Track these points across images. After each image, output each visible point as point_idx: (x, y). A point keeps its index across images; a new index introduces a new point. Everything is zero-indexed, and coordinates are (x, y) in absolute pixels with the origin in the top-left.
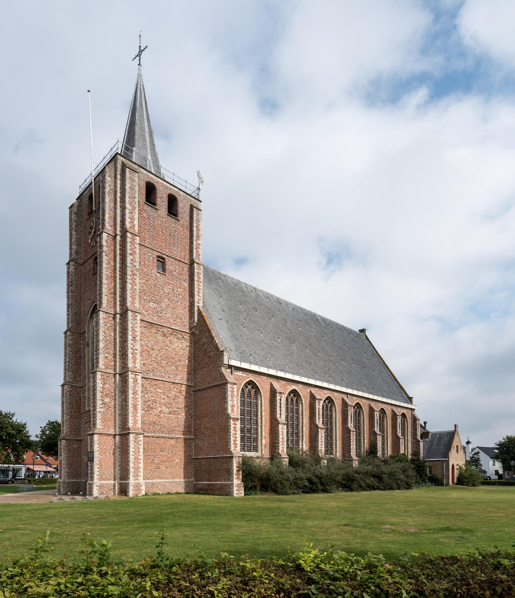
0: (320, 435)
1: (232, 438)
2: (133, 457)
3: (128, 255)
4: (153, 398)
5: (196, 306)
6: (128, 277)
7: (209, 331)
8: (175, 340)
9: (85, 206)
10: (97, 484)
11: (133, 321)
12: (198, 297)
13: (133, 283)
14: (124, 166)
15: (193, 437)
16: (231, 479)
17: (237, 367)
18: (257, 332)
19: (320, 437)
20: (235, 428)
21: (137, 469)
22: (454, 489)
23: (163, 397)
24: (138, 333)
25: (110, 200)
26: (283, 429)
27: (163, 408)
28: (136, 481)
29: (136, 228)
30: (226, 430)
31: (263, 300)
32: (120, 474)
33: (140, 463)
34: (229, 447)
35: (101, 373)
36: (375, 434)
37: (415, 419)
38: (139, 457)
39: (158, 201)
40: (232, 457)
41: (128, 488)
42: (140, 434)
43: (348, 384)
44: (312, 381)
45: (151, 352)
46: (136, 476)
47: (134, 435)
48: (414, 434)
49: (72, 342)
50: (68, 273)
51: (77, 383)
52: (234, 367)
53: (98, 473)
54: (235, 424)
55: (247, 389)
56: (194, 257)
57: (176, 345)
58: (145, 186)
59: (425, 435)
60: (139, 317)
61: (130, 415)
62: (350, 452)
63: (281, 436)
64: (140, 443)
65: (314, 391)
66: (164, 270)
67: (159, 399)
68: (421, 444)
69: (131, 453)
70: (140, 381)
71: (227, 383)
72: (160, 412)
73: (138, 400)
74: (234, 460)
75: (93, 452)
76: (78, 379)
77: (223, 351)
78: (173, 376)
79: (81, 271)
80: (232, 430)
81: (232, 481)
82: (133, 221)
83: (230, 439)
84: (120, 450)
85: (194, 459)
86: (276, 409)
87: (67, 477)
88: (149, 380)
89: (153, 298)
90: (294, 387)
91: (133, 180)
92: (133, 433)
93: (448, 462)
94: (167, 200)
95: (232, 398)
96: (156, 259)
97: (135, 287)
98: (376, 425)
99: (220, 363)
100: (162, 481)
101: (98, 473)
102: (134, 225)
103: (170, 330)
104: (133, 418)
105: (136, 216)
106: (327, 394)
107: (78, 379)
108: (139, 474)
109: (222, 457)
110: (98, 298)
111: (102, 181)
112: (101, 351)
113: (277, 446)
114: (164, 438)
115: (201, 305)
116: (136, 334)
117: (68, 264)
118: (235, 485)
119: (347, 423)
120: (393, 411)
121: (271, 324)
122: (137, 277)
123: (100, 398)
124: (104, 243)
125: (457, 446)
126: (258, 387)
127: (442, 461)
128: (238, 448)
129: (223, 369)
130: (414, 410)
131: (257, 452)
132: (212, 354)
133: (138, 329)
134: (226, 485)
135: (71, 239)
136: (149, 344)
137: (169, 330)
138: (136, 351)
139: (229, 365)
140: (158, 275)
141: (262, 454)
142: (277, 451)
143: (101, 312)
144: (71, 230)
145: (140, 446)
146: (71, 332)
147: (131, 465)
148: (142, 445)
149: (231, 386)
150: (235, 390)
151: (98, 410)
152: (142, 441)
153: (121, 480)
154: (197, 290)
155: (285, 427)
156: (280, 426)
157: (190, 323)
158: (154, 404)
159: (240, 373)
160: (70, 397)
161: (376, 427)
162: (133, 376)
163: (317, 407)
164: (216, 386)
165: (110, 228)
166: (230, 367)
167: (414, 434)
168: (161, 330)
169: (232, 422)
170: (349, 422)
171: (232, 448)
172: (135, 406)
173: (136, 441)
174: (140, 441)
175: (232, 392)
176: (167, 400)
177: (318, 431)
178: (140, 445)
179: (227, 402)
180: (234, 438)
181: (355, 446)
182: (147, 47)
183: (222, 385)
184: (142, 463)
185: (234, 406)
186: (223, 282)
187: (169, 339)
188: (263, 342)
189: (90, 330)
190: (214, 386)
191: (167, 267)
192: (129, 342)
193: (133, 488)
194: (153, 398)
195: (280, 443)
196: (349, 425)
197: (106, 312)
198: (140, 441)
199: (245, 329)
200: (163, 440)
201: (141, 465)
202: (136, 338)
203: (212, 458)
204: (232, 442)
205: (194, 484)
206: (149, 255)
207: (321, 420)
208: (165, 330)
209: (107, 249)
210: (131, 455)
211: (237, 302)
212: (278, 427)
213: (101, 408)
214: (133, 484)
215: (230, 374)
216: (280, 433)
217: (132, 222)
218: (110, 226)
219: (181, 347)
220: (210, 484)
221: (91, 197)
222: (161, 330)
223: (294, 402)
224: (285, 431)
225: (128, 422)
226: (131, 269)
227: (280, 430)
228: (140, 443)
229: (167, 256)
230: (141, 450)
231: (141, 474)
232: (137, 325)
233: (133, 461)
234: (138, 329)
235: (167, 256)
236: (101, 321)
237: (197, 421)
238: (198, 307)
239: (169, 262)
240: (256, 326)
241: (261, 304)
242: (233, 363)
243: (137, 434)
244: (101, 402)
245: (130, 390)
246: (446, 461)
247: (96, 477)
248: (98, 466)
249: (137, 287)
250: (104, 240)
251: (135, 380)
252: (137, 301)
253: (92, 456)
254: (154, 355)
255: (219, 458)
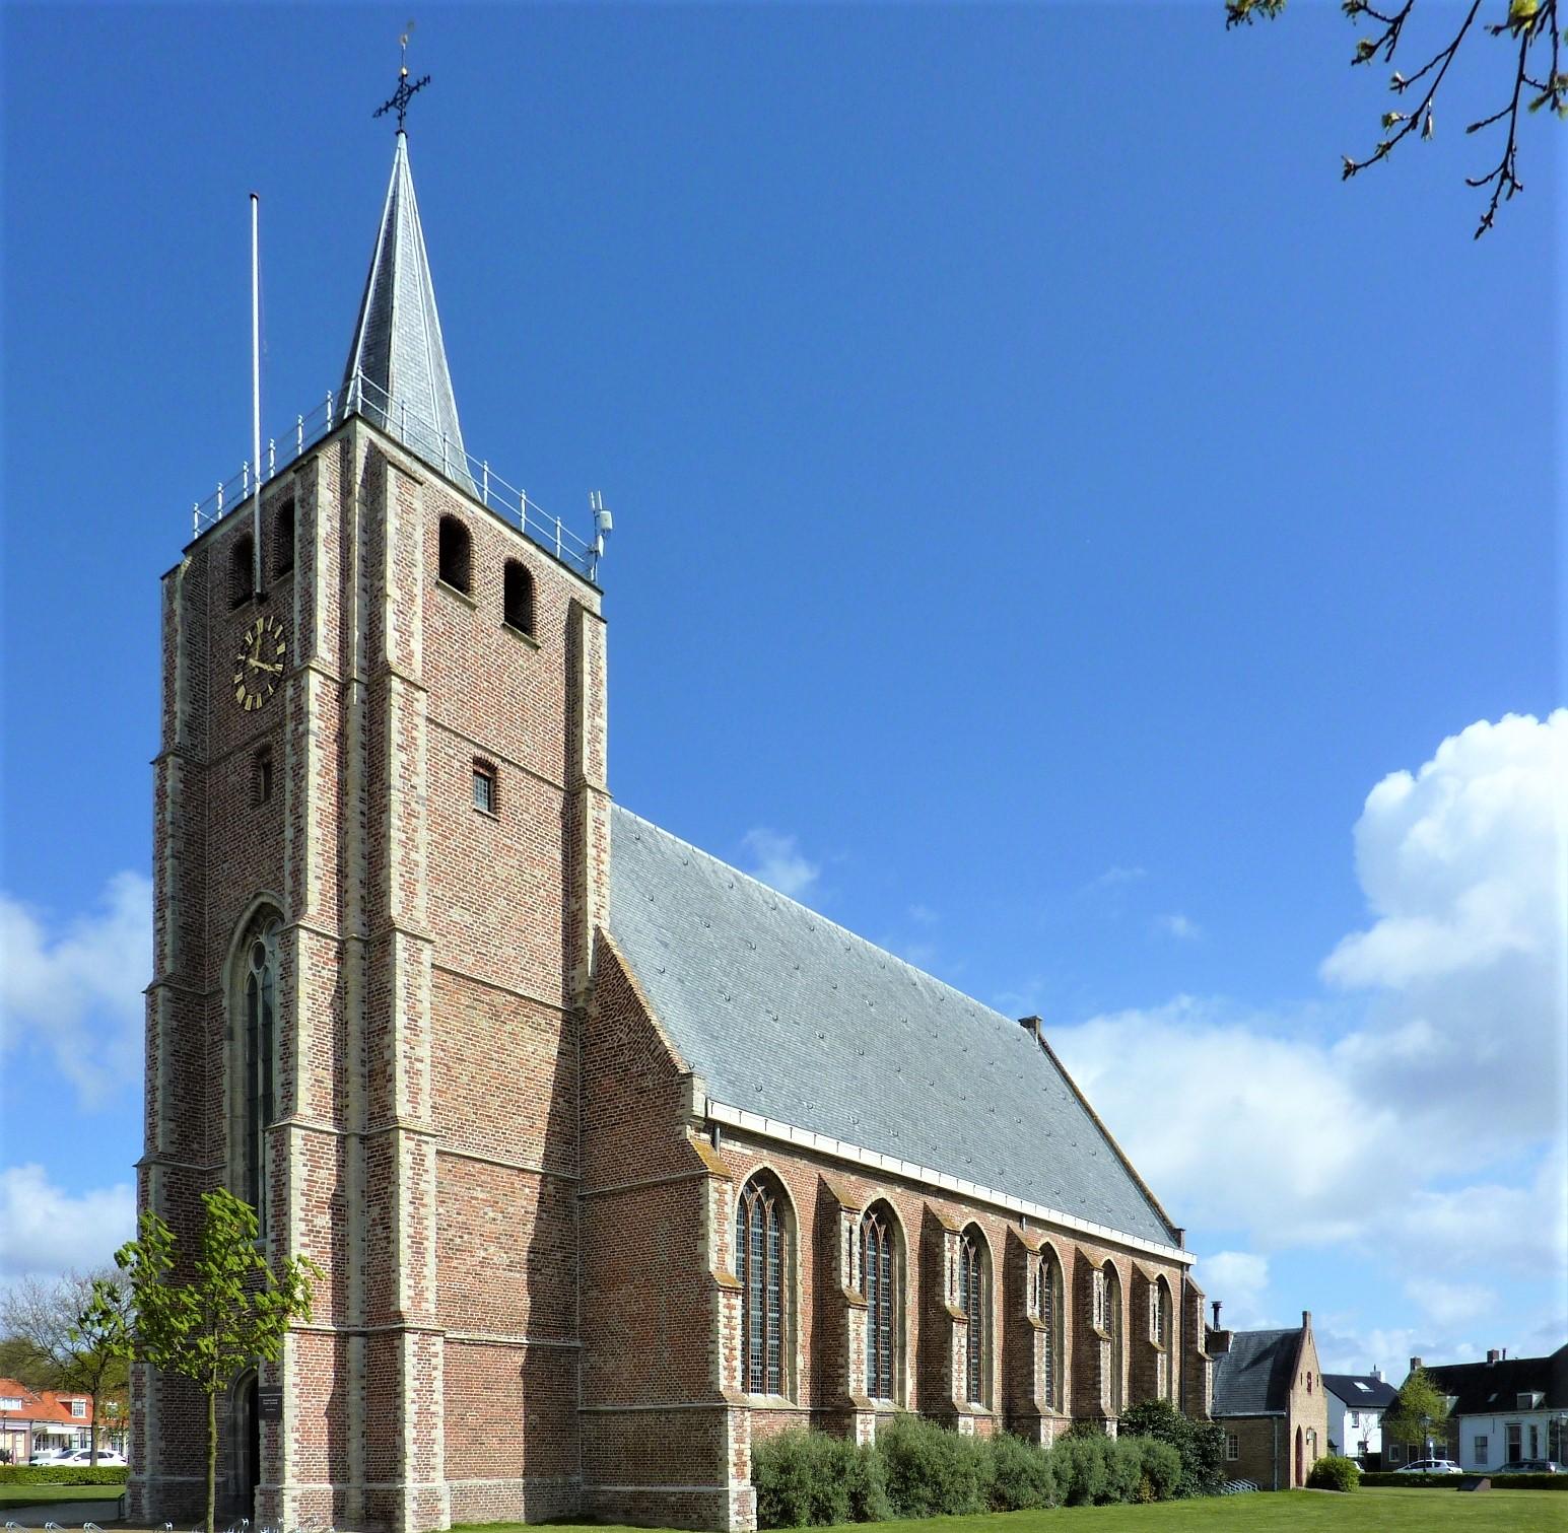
0: (955, 1341)
1: (721, 1350)
2: (415, 1407)
3: (394, 750)
4: (461, 1218)
5: (590, 925)
6: (395, 821)
7: (638, 1009)
8: (528, 1031)
9: (219, 575)
10: (294, 1493)
11: (408, 967)
12: (597, 899)
13: (409, 843)
14: (374, 454)
15: (578, 1343)
16: (719, 1477)
17: (732, 1127)
18: (763, 1017)
19: (955, 1349)
20: (730, 1318)
21: (425, 1444)
22: (1308, 1497)
23: (491, 1215)
24: (425, 1007)
25: (329, 570)
26: (859, 1324)
27: (492, 1250)
28: (425, 1485)
29: (417, 661)
30: (703, 1325)
31: (763, 914)
32: (366, 1462)
33: (434, 1427)
34: (711, 1378)
35: (303, 1132)
36: (1028, 1329)
37: (1190, 1295)
38: (433, 1408)
39: (478, 579)
40: (724, 1410)
41: (401, 1506)
42: (436, 1333)
43: (1017, 1185)
44: (930, 1177)
45: (457, 1069)
46: (425, 1469)
47: (416, 1337)
48: (1188, 1340)
49: (175, 1023)
50: (161, 794)
51: (191, 1160)
52: (723, 1125)
53: (297, 1458)
54: (730, 1307)
55: (754, 1196)
56: (585, 771)
57: (531, 1049)
58: (437, 527)
59: (1217, 1340)
60: (427, 955)
61: (404, 1271)
62: (1033, 1392)
63: (853, 1346)
64: (434, 1361)
65: (936, 1204)
66: (493, 803)
67: (479, 1221)
68: (1209, 1367)
69: (410, 1395)
70: (431, 1161)
71: (706, 1176)
72: (483, 1263)
73: (426, 1222)
74: (729, 1418)
75: (280, 1389)
76: (195, 1146)
77: (690, 1075)
78: (518, 1149)
79: (203, 790)
80: (721, 1326)
81: (724, 1483)
82: (407, 639)
83: (715, 1352)
84: (364, 1383)
85: (582, 1412)
86: (838, 1259)
87: (161, 1467)
88: (450, 1159)
89: (462, 894)
90: (882, 1192)
91: (408, 509)
92: (415, 1331)
93: (1286, 1421)
94: (502, 579)
95: (721, 1224)
96: (470, 767)
97: (413, 855)
98: (1096, 1312)
99: (679, 1112)
100: (489, 1482)
101: (297, 1458)
102: (411, 654)
103: (512, 999)
104: (411, 1282)
105: (417, 625)
106: (967, 1215)
107: (195, 1146)
108: (433, 1461)
109: (686, 1410)
110: (289, 883)
111: (302, 501)
112: (303, 1061)
113: (842, 1376)
114: (494, 1345)
115: (605, 925)
116: (420, 1008)
117: (160, 761)
118: (732, 1495)
119: (1024, 1304)
120: (1135, 1270)
121: (796, 994)
122: (421, 823)
123: (302, 1215)
124: (313, 706)
125: (1309, 1376)
126: (785, 1191)
127: (1270, 1417)
128: (737, 1384)
129: (690, 1132)
130: (1188, 1265)
131: (780, 1392)
132: (648, 1082)
133: (425, 995)
134: (699, 1496)
135: (168, 681)
136: (450, 1043)
137: (508, 997)
138: (418, 1065)
139: (706, 1119)
140: (479, 819)
141: (1019, 1418)
142: (840, 1390)
143: (302, 934)
144: (169, 652)
145: (434, 1374)
146: (171, 988)
147: (410, 1433)
148: (441, 1367)
149: (716, 1185)
150: (728, 1198)
151: (294, 1254)
152: (441, 1355)
153: (369, 1479)
154: (595, 873)
155: (738, 1302)
156: (852, 1314)
157: (567, 981)
158: (466, 1237)
159: (736, 1147)
160: (168, 1205)
161: (1096, 1319)
162: (411, 1145)
163: (948, 1255)
164: (664, 1183)
165: (329, 657)
166: (709, 1125)
167: (1188, 1340)
168: (486, 998)
169: (722, 1300)
170: (1029, 1303)
171: (723, 1383)
172: (418, 1243)
173: (424, 1356)
174: (436, 1355)
175: (721, 1203)
176: (501, 1226)
177: (950, 1330)
178: (435, 1369)
179: (704, 1237)
180: (727, 1351)
181: (1044, 1376)
182: (427, 80)
183: (692, 1180)
184: (441, 1425)
185: (722, 1251)
186: (650, 851)
187: (508, 1028)
188: (783, 1048)
189: (239, 988)
190: (656, 1185)
191: (503, 795)
192: (398, 1036)
193: (414, 1506)
194: (461, 1218)
195: (852, 1367)
196: (1029, 1312)
197: (318, 934)
198: (436, 1355)
199: (730, 1006)
200: (491, 1351)
201: (439, 1434)
202: (420, 1023)
203: (649, 1411)
204: (722, 1361)
205: (586, 1495)
206: (451, 752)
207: (957, 1294)
208: (499, 999)
209: (323, 725)
210: (408, 1401)
211: (697, 919)
212: (845, 1317)
213: (304, 1245)
214: (416, 1493)
215: (709, 1146)
216: (852, 1335)
217: (404, 643)
218: (330, 650)
219: (538, 1051)
220: (642, 1493)
221: (243, 549)
222: (486, 998)
223: (881, 1238)
224: (864, 1329)
225: (397, 1293)
226: (402, 796)
227: (852, 1326)
228: (434, 1361)
229: (504, 760)
230: (438, 1385)
231: (438, 1461)
232: (420, 981)
233: (415, 1418)
234: (425, 995)
235: (504, 760)
236: (304, 962)
237: (594, 1293)
238: (598, 929)
239: (508, 778)
240: (759, 997)
241: (761, 928)
242: (722, 1113)
243: (425, 1332)
244: (302, 1226)
245: (402, 1189)
246: (1281, 1417)
247: (290, 1469)
248: (297, 1435)
249: (420, 857)
250: (312, 697)
251: (419, 1160)
252: (421, 901)
253: (275, 1402)
254: (465, 1079)
255: (677, 1411)
